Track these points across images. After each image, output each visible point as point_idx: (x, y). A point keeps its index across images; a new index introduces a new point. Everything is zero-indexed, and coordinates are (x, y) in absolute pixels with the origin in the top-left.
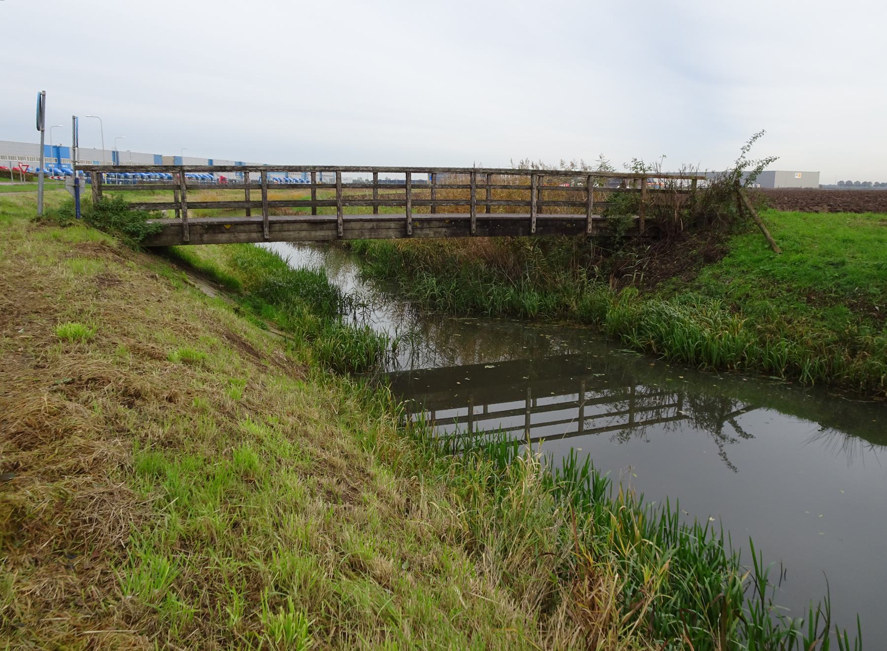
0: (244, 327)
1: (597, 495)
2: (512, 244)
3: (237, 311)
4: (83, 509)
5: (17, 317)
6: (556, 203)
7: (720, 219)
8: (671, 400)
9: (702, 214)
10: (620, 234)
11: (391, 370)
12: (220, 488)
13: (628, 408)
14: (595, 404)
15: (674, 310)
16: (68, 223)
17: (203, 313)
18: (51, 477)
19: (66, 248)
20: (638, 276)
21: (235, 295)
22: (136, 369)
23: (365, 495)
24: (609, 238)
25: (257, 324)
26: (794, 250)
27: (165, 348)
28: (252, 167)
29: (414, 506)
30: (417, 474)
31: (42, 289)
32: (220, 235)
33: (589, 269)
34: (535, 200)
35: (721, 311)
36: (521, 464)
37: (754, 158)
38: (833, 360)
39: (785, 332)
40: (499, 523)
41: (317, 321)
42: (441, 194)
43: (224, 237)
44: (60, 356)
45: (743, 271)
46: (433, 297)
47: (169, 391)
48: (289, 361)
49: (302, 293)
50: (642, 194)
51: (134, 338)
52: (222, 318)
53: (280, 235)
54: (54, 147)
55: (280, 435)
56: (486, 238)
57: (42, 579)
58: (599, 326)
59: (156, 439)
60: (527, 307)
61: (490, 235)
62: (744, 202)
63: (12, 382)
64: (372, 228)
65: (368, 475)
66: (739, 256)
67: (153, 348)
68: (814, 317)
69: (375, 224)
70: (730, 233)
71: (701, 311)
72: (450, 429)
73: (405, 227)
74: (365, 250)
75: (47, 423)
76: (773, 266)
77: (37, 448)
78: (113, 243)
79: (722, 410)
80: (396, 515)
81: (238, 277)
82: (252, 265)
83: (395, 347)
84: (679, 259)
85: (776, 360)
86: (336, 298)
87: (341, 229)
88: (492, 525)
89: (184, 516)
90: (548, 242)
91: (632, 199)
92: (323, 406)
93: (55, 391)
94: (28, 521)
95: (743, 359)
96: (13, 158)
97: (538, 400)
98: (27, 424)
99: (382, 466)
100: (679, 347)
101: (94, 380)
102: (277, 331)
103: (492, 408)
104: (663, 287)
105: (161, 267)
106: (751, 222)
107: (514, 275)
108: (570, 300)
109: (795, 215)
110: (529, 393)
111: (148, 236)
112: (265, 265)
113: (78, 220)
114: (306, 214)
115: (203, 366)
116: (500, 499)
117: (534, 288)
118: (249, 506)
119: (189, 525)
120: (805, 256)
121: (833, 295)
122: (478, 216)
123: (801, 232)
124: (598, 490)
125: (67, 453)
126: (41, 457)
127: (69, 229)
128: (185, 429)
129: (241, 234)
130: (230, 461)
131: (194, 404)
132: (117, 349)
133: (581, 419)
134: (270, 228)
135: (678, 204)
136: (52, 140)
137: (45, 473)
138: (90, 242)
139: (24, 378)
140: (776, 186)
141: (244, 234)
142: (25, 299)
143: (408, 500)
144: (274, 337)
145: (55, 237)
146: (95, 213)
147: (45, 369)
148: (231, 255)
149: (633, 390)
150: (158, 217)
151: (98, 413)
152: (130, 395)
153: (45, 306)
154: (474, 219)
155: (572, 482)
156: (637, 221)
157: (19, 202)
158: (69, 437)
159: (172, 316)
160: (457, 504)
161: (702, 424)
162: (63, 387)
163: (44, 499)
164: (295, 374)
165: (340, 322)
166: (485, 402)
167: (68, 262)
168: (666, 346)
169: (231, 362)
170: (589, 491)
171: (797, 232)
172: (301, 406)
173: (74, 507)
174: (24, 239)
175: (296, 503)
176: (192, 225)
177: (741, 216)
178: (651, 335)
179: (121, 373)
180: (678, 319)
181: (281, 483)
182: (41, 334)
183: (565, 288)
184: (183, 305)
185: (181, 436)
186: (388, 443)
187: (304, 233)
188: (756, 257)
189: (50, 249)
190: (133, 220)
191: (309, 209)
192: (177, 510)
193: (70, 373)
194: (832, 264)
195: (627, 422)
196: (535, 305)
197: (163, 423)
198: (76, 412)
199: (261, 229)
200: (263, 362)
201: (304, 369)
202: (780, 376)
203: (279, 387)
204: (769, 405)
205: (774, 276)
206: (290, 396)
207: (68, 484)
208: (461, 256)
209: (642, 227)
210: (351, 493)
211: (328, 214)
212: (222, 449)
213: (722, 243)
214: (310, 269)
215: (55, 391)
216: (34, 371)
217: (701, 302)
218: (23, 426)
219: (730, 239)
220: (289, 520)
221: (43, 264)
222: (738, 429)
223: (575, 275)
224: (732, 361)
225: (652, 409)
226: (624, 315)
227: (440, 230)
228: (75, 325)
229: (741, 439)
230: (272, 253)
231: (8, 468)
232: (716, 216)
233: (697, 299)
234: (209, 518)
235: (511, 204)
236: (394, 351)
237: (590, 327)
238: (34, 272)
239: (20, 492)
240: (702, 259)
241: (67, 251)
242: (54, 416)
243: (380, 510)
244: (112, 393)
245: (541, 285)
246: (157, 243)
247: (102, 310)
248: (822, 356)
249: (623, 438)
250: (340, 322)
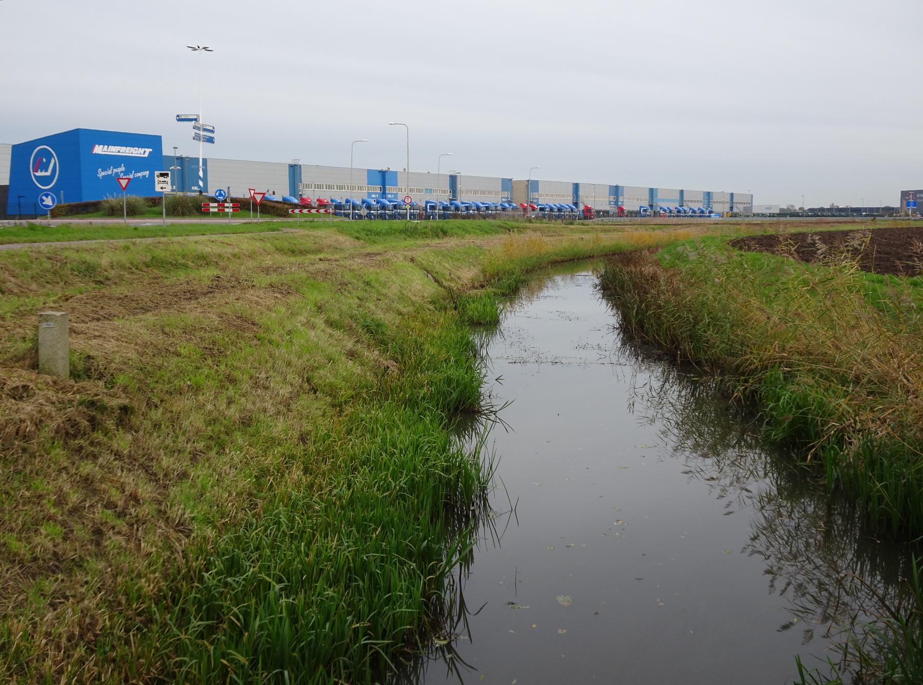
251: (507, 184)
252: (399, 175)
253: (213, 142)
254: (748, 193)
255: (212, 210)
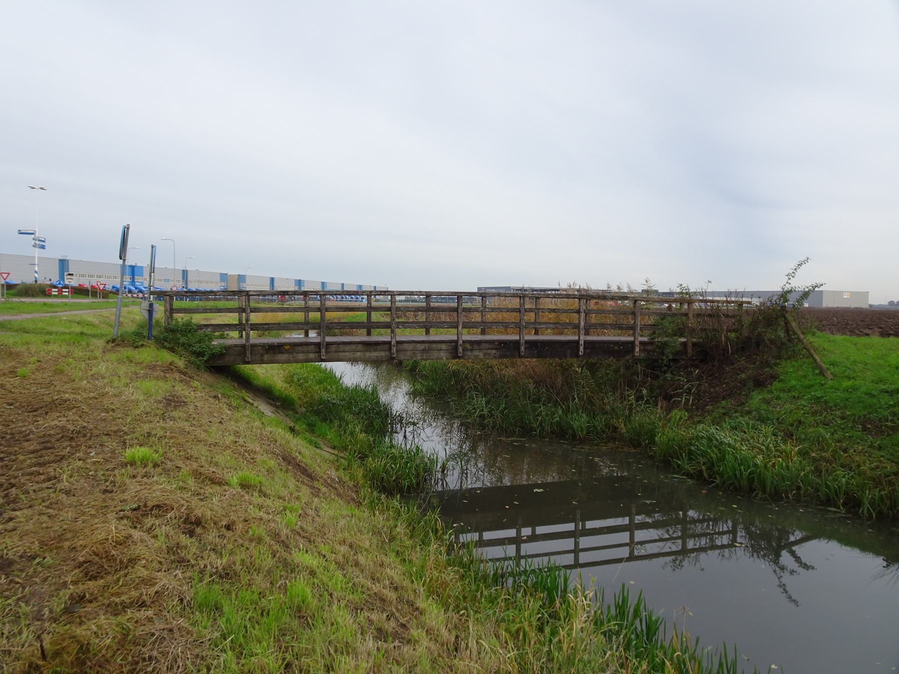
0: (299, 447)
1: (650, 636)
2: (561, 365)
3: (292, 430)
4: (144, 646)
5: (90, 439)
6: (603, 326)
7: (768, 343)
8: (725, 525)
9: (749, 338)
10: (668, 357)
11: (440, 489)
12: (274, 626)
13: (680, 534)
14: (647, 529)
15: (725, 436)
16: (140, 344)
17: (261, 434)
18: (115, 610)
19: (138, 369)
20: (687, 400)
21: (291, 413)
22: (197, 494)
23: (415, 633)
24: (656, 360)
25: (310, 442)
26: (846, 376)
27: (225, 472)
28: (312, 292)
29: (463, 645)
30: (466, 609)
31: (113, 410)
32: (279, 355)
33: (637, 391)
34: (582, 324)
35: (773, 437)
36: (571, 603)
37: (801, 283)
38: (893, 492)
39: (841, 461)
40: (550, 666)
41: (369, 440)
42: (490, 317)
43: (284, 357)
44: (128, 481)
45: (794, 397)
46: (482, 417)
47: (228, 519)
48: (340, 480)
49: (355, 411)
50: (688, 318)
51: (196, 462)
52: (278, 438)
53: (335, 355)
54: (130, 266)
55: (333, 567)
56: (534, 360)
57: (10, 423)
58: (648, 450)
59: (214, 570)
60: (576, 428)
61: (538, 357)
62: (792, 327)
63: (82, 508)
64: (424, 350)
65: (417, 609)
66: (790, 381)
67: (214, 472)
68: (871, 446)
69: (427, 345)
70: (779, 357)
71: (752, 437)
72: (497, 552)
73: (456, 348)
74: (416, 367)
75: (113, 552)
76: (825, 392)
77: (102, 578)
78: (181, 363)
79: (780, 539)
80: (445, 655)
81: (294, 393)
82: (308, 382)
83: (444, 468)
84: (727, 383)
85: (833, 491)
86: (387, 414)
87: (394, 350)
88: (542, 668)
89: (239, 656)
90: (596, 363)
91: (678, 323)
92: (374, 533)
93: (122, 518)
94: (91, 657)
95: (799, 488)
96: (92, 276)
97: (587, 523)
98: (94, 552)
99: (431, 598)
100: (731, 474)
101: (158, 507)
102: (330, 450)
103: (541, 530)
104: (713, 411)
105: (224, 386)
106: (800, 347)
107: (562, 395)
108: (618, 422)
109: (845, 339)
110: (578, 517)
111: (213, 356)
112: (320, 382)
113: (150, 342)
114: (361, 336)
115: (260, 491)
116: (550, 641)
117: (583, 410)
118: (301, 646)
119: (243, 665)
120: (857, 383)
121: (889, 424)
122: (527, 338)
123: (852, 358)
124: (651, 629)
125: (130, 585)
126: (106, 588)
127: (141, 349)
128: (243, 561)
129: (299, 355)
130: (284, 595)
131: (251, 533)
132: (181, 473)
133: (631, 544)
134: (326, 349)
135: (725, 328)
136: (130, 261)
137: (109, 605)
138: (159, 363)
139: (93, 503)
140: (824, 305)
141: (302, 355)
142: (98, 421)
143: (457, 637)
144: (327, 455)
145: (128, 357)
146: (166, 334)
147: (113, 494)
148: (287, 371)
149: (685, 515)
150: (222, 337)
151: (161, 543)
152: (191, 523)
153: (116, 428)
154: (522, 342)
155: (625, 623)
156: (684, 344)
157: (95, 321)
158: (133, 568)
159: (232, 438)
160: (506, 642)
161: (758, 553)
162: (129, 513)
163: (107, 634)
164: (346, 496)
165: (391, 441)
166: (533, 524)
167: (138, 383)
168: (717, 473)
169: (286, 486)
170: (642, 630)
171: (848, 358)
172: (353, 533)
173: (136, 644)
174: (100, 359)
175: (347, 643)
176: (254, 346)
177: (790, 340)
178: (702, 460)
179: (184, 499)
180: (729, 445)
181: (333, 620)
182: (110, 457)
183: (613, 410)
184: (242, 426)
185: (238, 567)
186: (437, 574)
187: (359, 354)
188: (807, 383)
189: (122, 370)
190: (199, 342)
191: (364, 331)
192: (233, 649)
193: (136, 499)
194: (887, 392)
195: (680, 548)
196: (583, 426)
197: (221, 553)
198: (141, 541)
199: (318, 350)
200: (316, 484)
201: (355, 489)
202: (839, 508)
203: (331, 513)
204: (830, 537)
205: (826, 402)
206: (342, 522)
207: (131, 618)
208: (509, 376)
209: (690, 350)
210: (400, 630)
211: (382, 336)
212: (277, 582)
213: (772, 367)
214: (363, 385)
215: (122, 518)
216: (103, 496)
217: (752, 428)
218: (91, 555)
219: (779, 364)
220: (340, 662)
221: (115, 385)
222: (797, 559)
223: (623, 398)
224: (786, 490)
225: (705, 535)
226: (674, 439)
227: (489, 351)
228: (143, 449)
229: (801, 570)
230: (326, 369)
231: (75, 599)
232: (764, 340)
233: (748, 424)
234: (263, 658)
235: (559, 327)
236: (443, 471)
237: (638, 450)
238: (107, 393)
239: (85, 627)
240: (752, 383)
241: (138, 371)
242: (121, 544)
243: (429, 649)
244: (174, 521)
245: (589, 406)
246: (220, 363)
247: (168, 434)
248: (881, 487)
249: (677, 565)
250: (391, 441)
251: (224, 277)
252: (144, 269)
253: (44, 248)
254: (385, 286)
255: (53, 293)
